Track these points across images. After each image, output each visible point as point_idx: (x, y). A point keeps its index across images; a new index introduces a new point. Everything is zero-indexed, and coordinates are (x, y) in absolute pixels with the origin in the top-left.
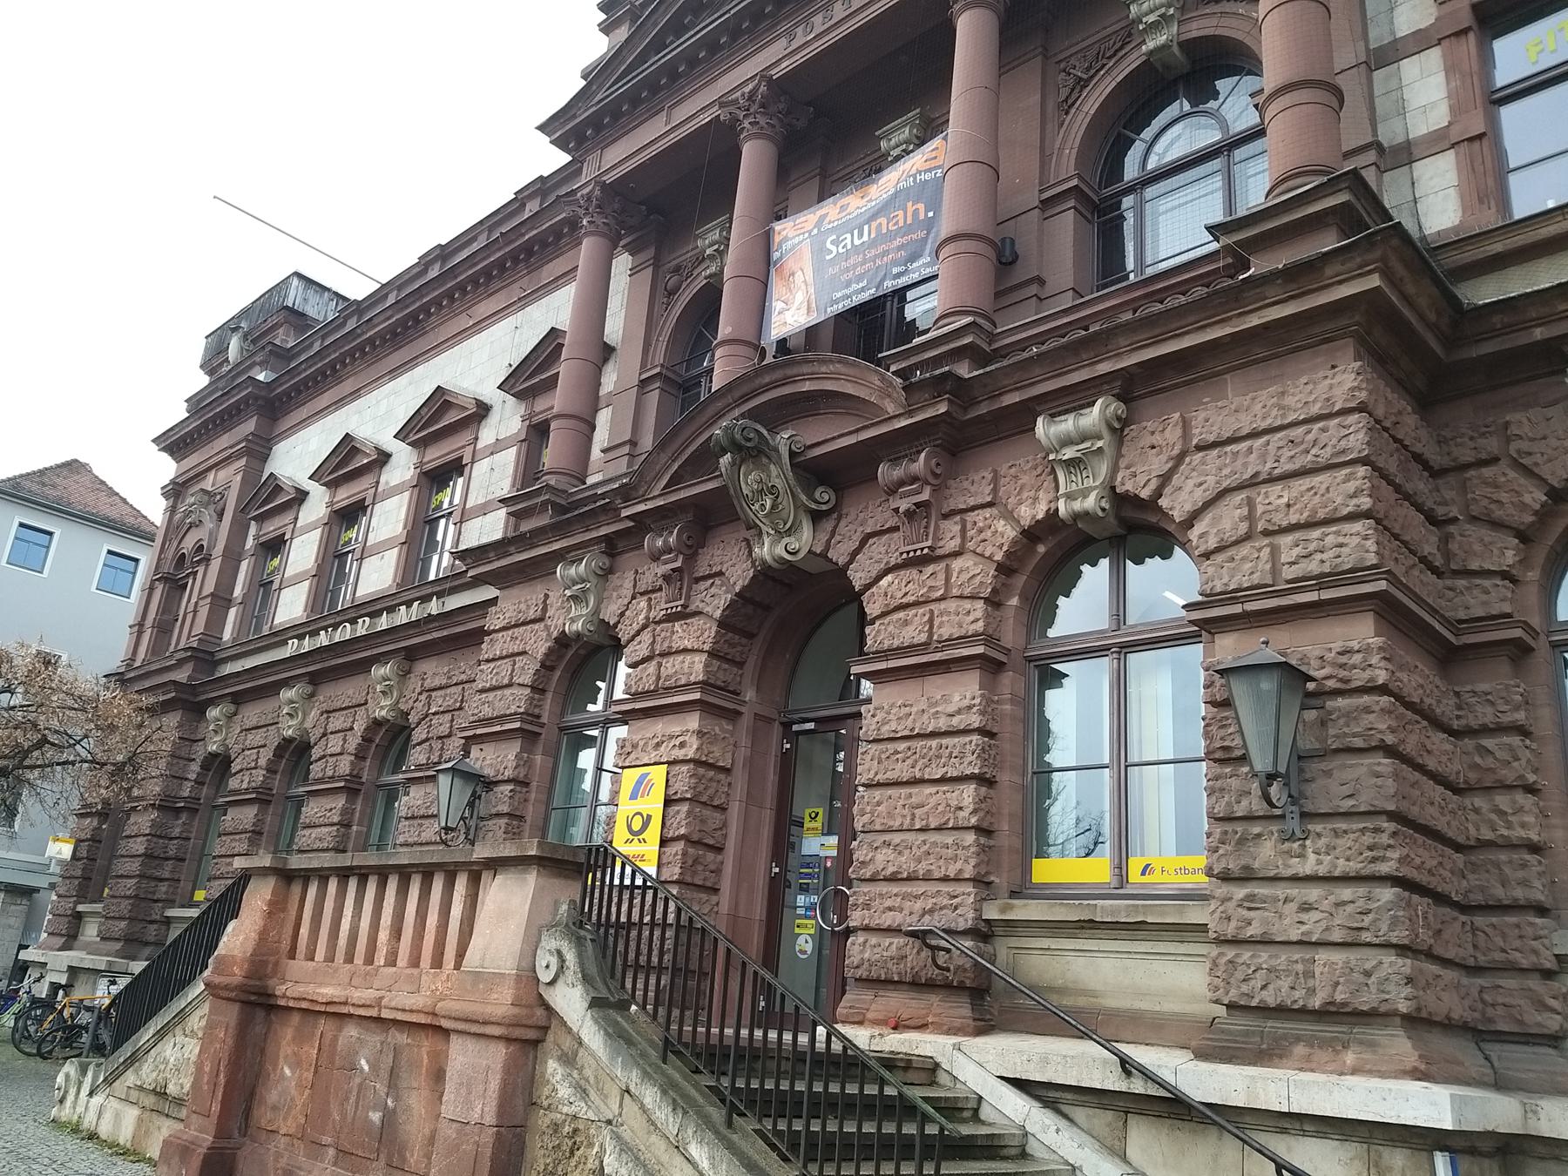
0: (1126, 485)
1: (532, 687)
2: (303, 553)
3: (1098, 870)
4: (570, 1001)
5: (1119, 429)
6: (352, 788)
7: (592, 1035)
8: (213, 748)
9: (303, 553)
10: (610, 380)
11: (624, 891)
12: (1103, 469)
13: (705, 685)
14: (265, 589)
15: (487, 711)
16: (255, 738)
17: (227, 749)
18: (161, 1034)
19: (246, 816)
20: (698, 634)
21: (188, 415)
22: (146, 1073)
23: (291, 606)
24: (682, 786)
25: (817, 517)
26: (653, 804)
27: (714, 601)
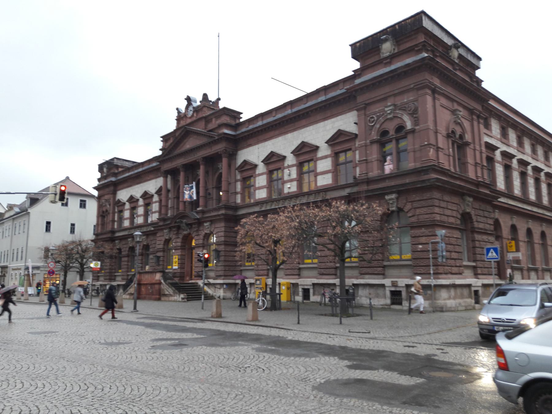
0: (399, 206)
1: (224, 236)
2: (127, 214)
3: (397, 257)
4: (162, 281)
5: (397, 199)
6: (128, 256)
7: (164, 283)
8: (131, 246)
9: (127, 214)
10: (170, 195)
11: (314, 262)
12: (395, 204)
13: (181, 246)
14: (121, 219)
15: (159, 248)
16: (125, 246)
17: (148, 244)
18: (130, 288)
19: (126, 259)
20: (179, 240)
21: (357, 65)
22: (129, 292)
23: (126, 224)
24: (180, 258)
25: (189, 229)
26: (177, 260)
27: (181, 236)
